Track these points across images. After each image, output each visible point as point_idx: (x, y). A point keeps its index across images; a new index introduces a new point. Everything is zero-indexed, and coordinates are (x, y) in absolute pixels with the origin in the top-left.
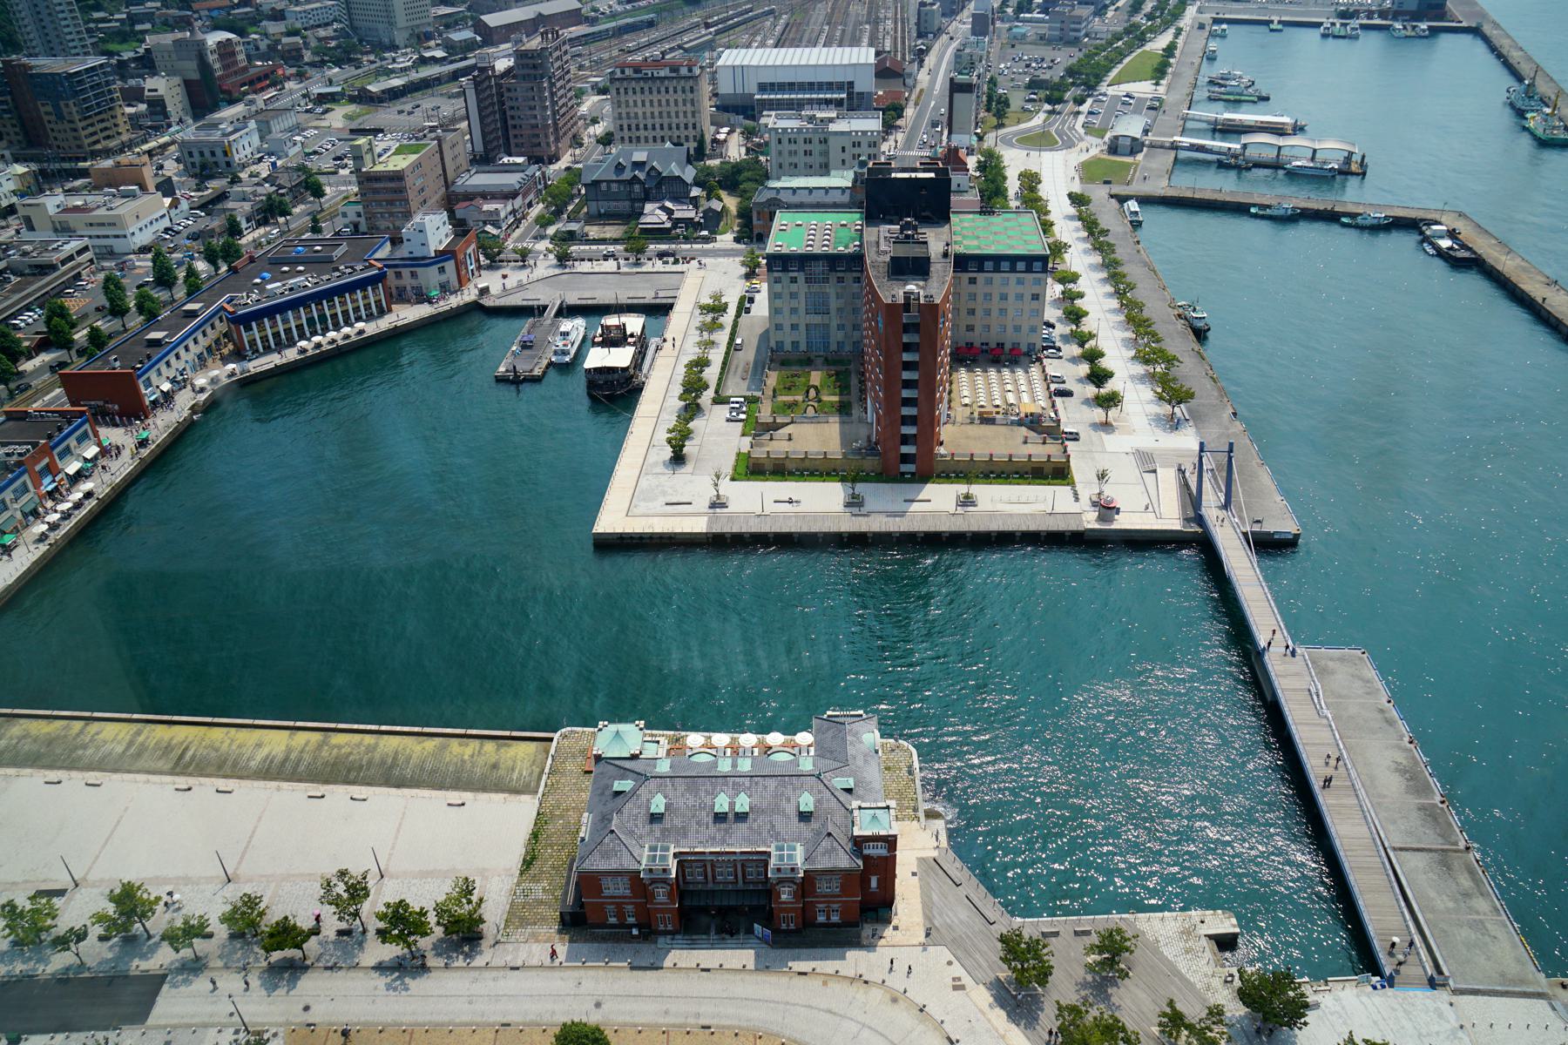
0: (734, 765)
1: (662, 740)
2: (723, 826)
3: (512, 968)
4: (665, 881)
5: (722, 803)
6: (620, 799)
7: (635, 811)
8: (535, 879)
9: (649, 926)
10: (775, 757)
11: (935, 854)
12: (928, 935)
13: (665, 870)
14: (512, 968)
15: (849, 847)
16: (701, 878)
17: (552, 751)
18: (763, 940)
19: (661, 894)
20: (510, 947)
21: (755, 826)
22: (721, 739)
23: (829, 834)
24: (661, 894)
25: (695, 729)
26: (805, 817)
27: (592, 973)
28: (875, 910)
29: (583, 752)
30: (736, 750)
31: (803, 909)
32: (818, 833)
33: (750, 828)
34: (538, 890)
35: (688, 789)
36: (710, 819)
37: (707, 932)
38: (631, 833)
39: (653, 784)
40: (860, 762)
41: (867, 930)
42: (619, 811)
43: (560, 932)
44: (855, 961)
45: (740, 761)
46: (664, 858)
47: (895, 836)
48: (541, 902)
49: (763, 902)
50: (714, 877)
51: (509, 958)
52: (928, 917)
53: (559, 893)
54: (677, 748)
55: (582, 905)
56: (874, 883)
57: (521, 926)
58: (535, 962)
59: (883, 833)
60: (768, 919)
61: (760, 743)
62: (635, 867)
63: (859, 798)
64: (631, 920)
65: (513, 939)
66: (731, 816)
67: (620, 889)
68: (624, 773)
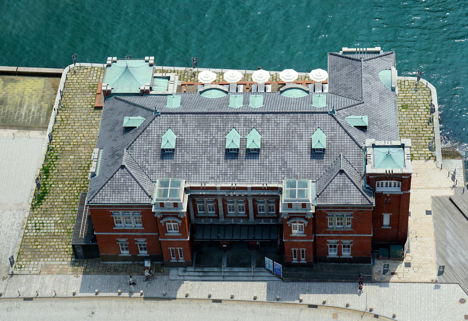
0: (246, 102)
1: (172, 75)
2: (234, 162)
3: (25, 299)
4: (176, 215)
5: (233, 140)
6: (130, 136)
7: (146, 147)
8: (46, 213)
9: (161, 259)
10: (288, 94)
11: (451, 193)
12: (440, 273)
13: (304, 206)
14: (25, 299)
15: (362, 184)
16: (243, 213)
17: (61, 87)
18: (273, 273)
19: (173, 230)
20: (23, 279)
21: (267, 162)
22: (233, 76)
23: (342, 172)
24: (173, 230)
25: (211, 66)
26: (317, 154)
27: (104, 303)
28: (387, 247)
29: (93, 87)
30: (249, 87)
31: (314, 244)
32: (330, 170)
33: (262, 165)
34: (51, 224)
35: (199, 126)
36: (222, 155)
37: (219, 265)
38: (142, 168)
39: (163, 120)
40: (375, 100)
41: (378, 266)
42: (129, 147)
43: (73, 264)
44: (370, 296)
45: (252, 97)
46: (175, 193)
47: (409, 175)
48: (53, 236)
49: (274, 237)
50: (225, 211)
51: (22, 289)
52: (441, 255)
53: (71, 227)
54: (188, 86)
55: (94, 239)
56: (386, 220)
57: (34, 258)
58: (48, 292)
59: (397, 171)
60: (280, 254)
61: (274, 79)
62: (146, 201)
63: (373, 136)
64: (143, 253)
65: (26, 271)
66: (242, 153)
67: (132, 222)
68: (134, 109)
